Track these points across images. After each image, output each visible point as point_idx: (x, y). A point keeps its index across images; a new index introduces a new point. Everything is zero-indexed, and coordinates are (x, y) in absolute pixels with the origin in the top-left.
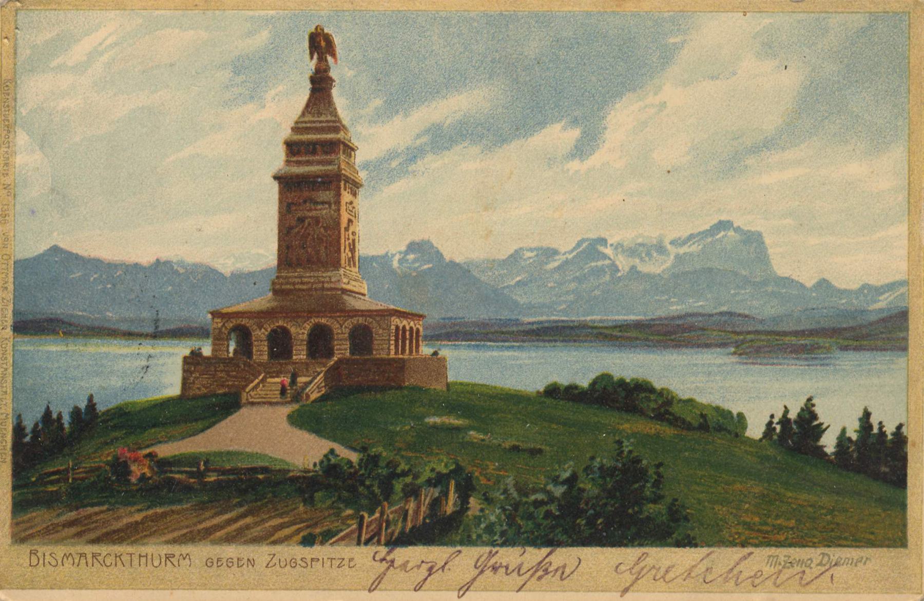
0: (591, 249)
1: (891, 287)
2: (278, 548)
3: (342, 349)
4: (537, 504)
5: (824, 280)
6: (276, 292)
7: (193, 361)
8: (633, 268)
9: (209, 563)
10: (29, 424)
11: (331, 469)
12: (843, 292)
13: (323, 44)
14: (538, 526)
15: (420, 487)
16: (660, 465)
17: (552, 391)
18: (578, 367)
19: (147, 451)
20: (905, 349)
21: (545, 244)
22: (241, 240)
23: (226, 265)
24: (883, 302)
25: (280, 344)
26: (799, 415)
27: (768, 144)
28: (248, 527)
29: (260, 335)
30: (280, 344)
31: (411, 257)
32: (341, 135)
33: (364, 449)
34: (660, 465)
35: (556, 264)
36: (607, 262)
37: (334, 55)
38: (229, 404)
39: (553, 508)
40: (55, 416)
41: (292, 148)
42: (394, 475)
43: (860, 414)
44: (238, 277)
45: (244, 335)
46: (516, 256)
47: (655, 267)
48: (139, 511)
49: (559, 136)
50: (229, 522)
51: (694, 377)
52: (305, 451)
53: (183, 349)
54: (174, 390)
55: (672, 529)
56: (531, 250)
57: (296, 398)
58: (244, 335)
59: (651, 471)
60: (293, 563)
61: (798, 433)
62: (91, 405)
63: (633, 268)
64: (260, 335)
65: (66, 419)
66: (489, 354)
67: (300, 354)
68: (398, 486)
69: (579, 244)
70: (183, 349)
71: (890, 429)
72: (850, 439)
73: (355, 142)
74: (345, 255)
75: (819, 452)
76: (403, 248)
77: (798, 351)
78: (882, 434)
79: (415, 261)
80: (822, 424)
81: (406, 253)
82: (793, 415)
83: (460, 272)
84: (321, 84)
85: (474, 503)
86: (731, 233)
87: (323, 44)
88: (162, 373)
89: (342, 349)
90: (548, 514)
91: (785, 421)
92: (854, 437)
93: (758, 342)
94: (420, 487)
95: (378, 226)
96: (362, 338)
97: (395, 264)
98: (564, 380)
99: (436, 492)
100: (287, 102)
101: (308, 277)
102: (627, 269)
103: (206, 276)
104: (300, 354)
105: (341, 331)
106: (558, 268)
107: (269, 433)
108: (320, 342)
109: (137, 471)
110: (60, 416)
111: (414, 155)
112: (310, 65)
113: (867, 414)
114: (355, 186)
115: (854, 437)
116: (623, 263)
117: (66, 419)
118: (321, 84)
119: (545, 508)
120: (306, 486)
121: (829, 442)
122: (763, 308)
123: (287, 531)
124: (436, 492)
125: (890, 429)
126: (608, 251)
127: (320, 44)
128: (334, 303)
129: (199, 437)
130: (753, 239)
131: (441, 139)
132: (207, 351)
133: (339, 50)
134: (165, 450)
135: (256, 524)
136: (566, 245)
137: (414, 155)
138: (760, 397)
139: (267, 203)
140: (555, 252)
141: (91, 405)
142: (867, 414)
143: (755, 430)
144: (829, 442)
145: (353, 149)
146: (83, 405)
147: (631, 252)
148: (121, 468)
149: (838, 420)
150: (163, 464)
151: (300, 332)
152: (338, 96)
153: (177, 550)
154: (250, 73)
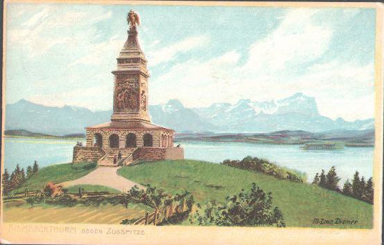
0: (244, 104)
1: (368, 121)
2: (110, 226)
3: (140, 144)
4: (220, 209)
5: (340, 118)
6: (112, 120)
7: (76, 150)
8: (262, 112)
9: (83, 231)
10: (10, 173)
11: (134, 193)
12: (350, 124)
13: (134, 18)
14: (220, 218)
15: (172, 200)
16: (270, 193)
17: (227, 163)
18: (238, 152)
19: (58, 185)
20: (373, 146)
21: (227, 102)
22: (99, 99)
23: (93, 108)
24: (364, 128)
25: (114, 141)
26: (329, 174)
27: (318, 61)
28: (100, 217)
29: (106, 138)
30: (114, 141)
31: (170, 106)
32: (141, 56)
33: (148, 185)
34: (270, 193)
35: (230, 110)
36: (251, 109)
37: (138, 23)
38: (92, 167)
39: (227, 211)
40: (21, 170)
41: (120, 61)
42: (161, 196)
43: (355, 173)
44: (98, 113)
45: (99, 137)
46: (213, 106)
47: (272, 111)
48: (86, 212)
49: (232, 56)
50: (91, 215)
51: (285, 158)
52: (124, 185)
53: (73, 143)
54: (70, 160)
55: (276, 219)
56: (220, 104)
57: (121, 164)
58: (99, 137)
59: (267, 196)
60: (118, 232)
61: (328, 181)
62: (36, 166)
63: (262, 112)
64: (106, 138)
65: (25, 171)
66: (283, 149)
67: (122, 144)
68: (163, 201)
69: (240, 101)
70: (73, 143)
71: (366, 180)
72: (350, 184)
73: (146, 58)
74: (142, 105)
75: (338, 190)
76: (167, 102)
77: (329, 147)
78: (363, 181)
79: (171, 108)
80: (29, 167)
81: (168, 104)
82: (326, 174)
83: (190, 113)
84: (132, 35)
85: (194, 207)
86: (302, 98)
87: (134, 18)
88: (63, 153)
89: (140, 144)
90: (224, 213)
91: (323, 176)
92: (352, 183)
93: (310, 142)
94: (172, 200)
95: (161, 96)
96: (148, 139)
97: (163, 108)
98: (232, 159)
99: (178, 203)
100: (119, 42)
101: (125, 116)
102: (259, 112)
103: (84, 112)
104: (122, 144)
105: (140, 136)
106: (231, 112)
107: (108, 177)
108: (131, 141)
109: (57, 192)
110: (23, 170)
111: (172, 63)
112: (128, 27)
113: (357, 173)
114: (146, 76)
115: (352, 183)
116: (258, 110)
117: (25, 171)
118: (132, 35)
119: (222, 210)
120: (123, 200)
121: (341, 185)
122: (316, 130)
123: (116, 219)
124: (178, 203)
125: (366, 180)
126: (251, 104)
127: (132, 18)
128: (137, 124)
129: (82, 178)
130: (311, 101)
131: (183, 57)
132: (84, 144)
133: (140, 21)
134: (67, 184)
135: (103, 216)
136: (234, 101)
137: (172, 63)
138: (310, 165)
139: (110, 83)
140: (230, 105)
141: (36, 166)
142: (357, 173)
143: (310, 179)
144: (341, 185)
145: (145, 61)
146: (32, 165)
147: (261, 105)
148: (49, 191)
149: (345, 176)
150: (65, 191)
151: (122, 136)
152: (139, 38)
153: (70, 225)
154: (103, 29)
